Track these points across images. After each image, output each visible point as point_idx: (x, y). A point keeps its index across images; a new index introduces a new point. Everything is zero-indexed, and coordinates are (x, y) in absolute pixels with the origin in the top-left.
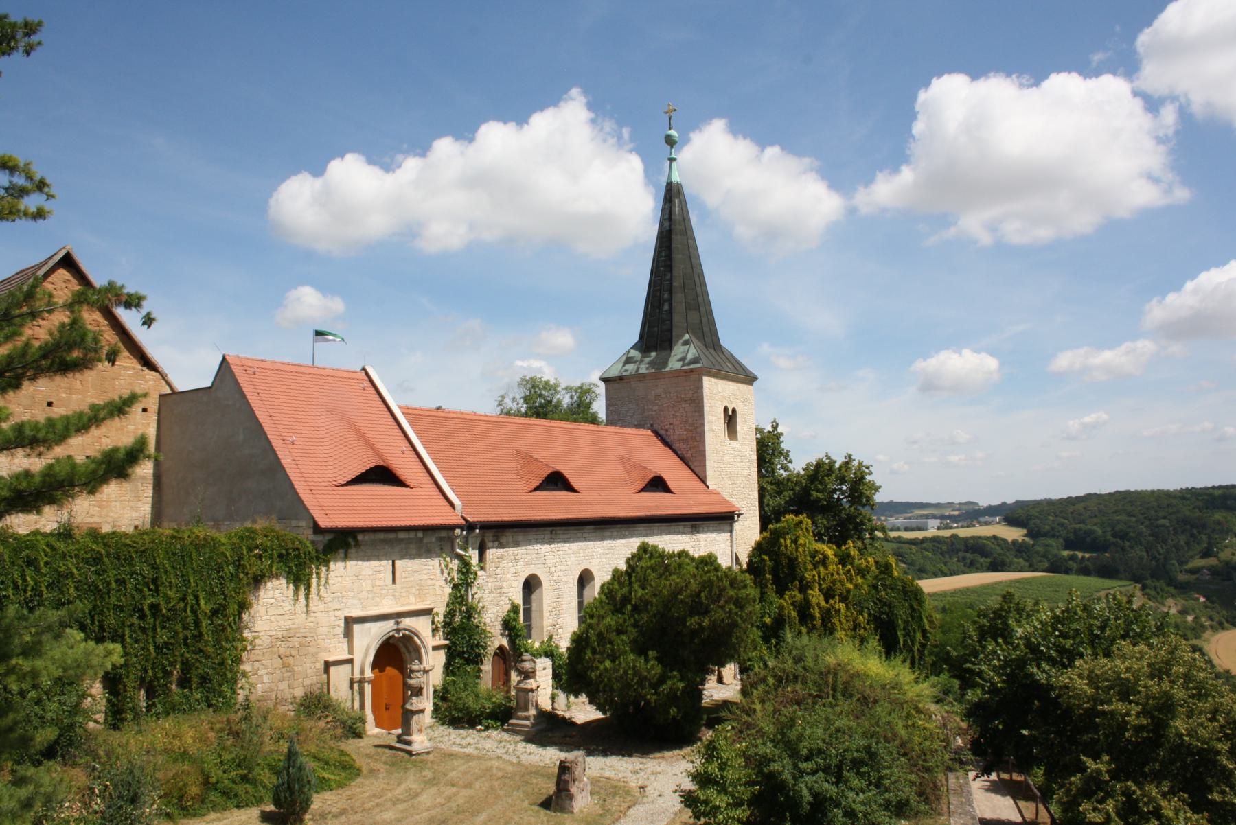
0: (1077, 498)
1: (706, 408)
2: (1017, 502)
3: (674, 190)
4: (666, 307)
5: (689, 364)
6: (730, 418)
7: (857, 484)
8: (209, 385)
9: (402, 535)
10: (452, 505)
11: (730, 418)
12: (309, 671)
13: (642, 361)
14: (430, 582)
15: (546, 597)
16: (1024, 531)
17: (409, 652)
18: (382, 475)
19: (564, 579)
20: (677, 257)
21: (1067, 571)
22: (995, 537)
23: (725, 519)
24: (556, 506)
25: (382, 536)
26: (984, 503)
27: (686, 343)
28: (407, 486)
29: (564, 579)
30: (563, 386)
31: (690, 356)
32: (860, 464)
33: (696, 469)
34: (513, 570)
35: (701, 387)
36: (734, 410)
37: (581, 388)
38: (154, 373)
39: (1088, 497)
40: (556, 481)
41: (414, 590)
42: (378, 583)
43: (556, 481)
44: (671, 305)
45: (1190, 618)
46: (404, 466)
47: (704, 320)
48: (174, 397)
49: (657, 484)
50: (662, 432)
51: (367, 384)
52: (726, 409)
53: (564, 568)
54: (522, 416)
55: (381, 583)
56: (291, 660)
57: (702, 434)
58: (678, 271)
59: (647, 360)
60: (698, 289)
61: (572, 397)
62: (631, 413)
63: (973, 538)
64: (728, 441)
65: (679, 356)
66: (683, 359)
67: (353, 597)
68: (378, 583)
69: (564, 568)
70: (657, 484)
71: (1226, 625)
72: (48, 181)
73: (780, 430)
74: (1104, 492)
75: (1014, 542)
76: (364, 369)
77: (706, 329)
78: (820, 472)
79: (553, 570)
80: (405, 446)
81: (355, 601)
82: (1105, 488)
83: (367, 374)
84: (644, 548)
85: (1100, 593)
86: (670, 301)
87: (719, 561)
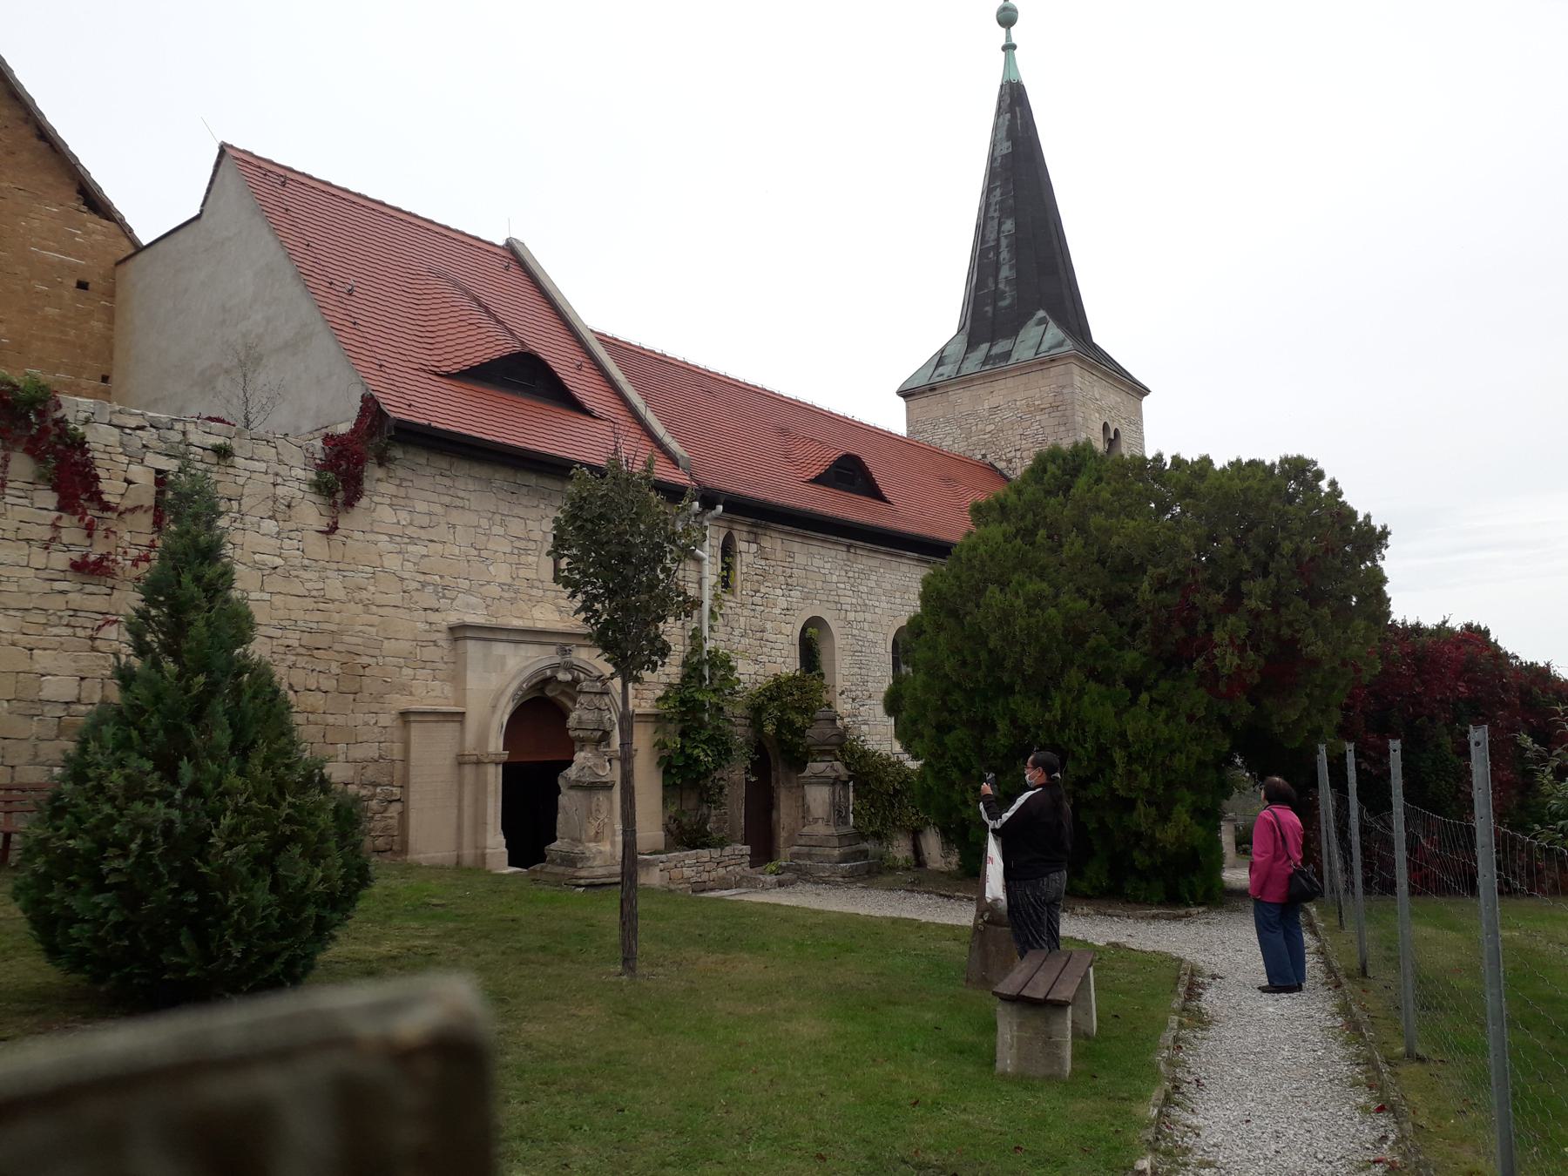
27: (1042, 321)
34: (782, 602)
38: (105, 222)
42: (523, 573)
50: (1001, 465)
67: (468, 592)
68: (523, 573)
79: (851, 616)
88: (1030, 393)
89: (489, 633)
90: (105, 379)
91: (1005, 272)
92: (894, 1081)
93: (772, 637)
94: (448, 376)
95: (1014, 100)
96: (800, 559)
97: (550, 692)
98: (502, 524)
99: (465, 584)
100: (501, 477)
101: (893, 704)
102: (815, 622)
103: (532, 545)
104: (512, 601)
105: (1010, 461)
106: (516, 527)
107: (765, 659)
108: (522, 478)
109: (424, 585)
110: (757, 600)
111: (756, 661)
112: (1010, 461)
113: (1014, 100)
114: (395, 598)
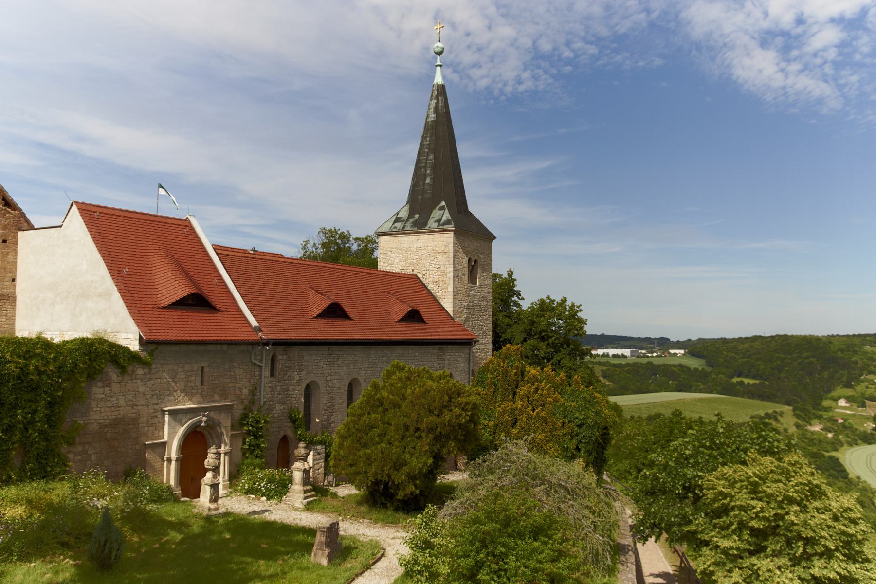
0: (746, 338)
2: (699, 339)
5: (443, 225)
7: (573, 318)
9: (211, 347)
13: (407, 221)
14: (231, 385)
15: (321, 400)
16: (703, 361)
17: (212, 438)
19: (337, 385)
21: (736, 394)
22: (681, 365)
24: (415, 332)
25: (193, 347)
26: (673, 339)
27: (442, 208)
29: (337, 385)
30: (354, 236)
31: (444, 219)
32: (573, 305)
34: (297, 378)
37: (366, 238)
39: (756, 338)
45: (830, 435)
59: (412, 220)
61: (359, 245)
62: (397, 260)
63: (664, 365)
65: (436, 219)
66: (439, 221)
69: (337, 377)
71: (859, 442)
73: (514, 277)
74: (768, 334)
75: (696, 370)
78: (545, 307)
79: (329, 378)
82: (768, 331)
85: (741, 411)
87: (132, 349)
88: (434, 244)
90: (14, 280)
91: (428, 180)
92: (136, 496)
94: (164, 308)
96: (306, 358)
97: (198, 430)
98: (182, 367)
102: (313, 383)
106: (187, 367)
109: (153, 395)
114: (142, 402)
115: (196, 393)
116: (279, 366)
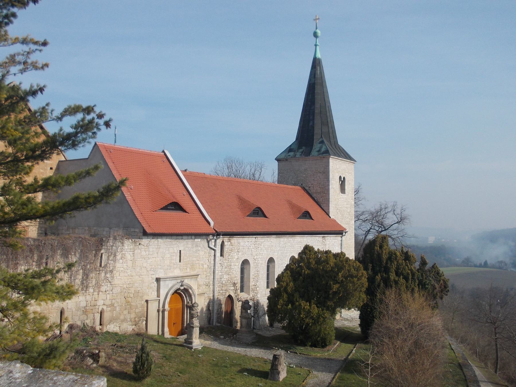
1: (331, 177)
3: (317, 62)
4: (311, 124)
6: (342, 182)
8: (87, 157)
10: (209, 223)
11: (342, 182)
12: (138, 305)
14: (197, 262)
18: (176, 206)
20: (318, 97)
23: (340, 232)
28: (186, 212)
29: (261, 262)
33: (324, 208)
34: (236, 257)
35: (328, 166)
36: (344, 178)
40: (258, 212)
41: (189, 265)
42: (172, 262)
43: (258, 212)
44: (313, 122)
46: (185, 203)
47: (331, 131)
48: (67, 162)
49: (306, 215)
50: (307, 188)
51: (165, 159)
52: (340, 177)
53: (260, 257)
54: (483, 267)
55: (174, 262)
56: (130, 299)
57: (328, 190)
58: (317, 106)
59: (301, 150)
60: (328, 114)
64: (341, 194)
65: (318, 149)
67: (161, 269)
68: (172, 262)
69: (260, 257)
70: (306, 215)
72: (49, 66)
76: (163, 152)
77: (331, 135)
79: (255, 257)
80: (185, 193)
81: (161, 271)
83: (165, 155)
84: (307, 249)
86: (313, 119)
89: (165, 279)
93: (233, 267)
95: (316, 64)
96: (242, 244)
99: (160, 267)
100: (175, 237)
101: (278, 276)
103: (175, 254)
104: (170, 269)
105: (310, 187)
107: (231, 273)
108: (164, 237)
110: (229, 257)
111: (228, 275)
112: (310, 187)
113: (316, 64)
115: (176, 267)
116: (226, 249)
